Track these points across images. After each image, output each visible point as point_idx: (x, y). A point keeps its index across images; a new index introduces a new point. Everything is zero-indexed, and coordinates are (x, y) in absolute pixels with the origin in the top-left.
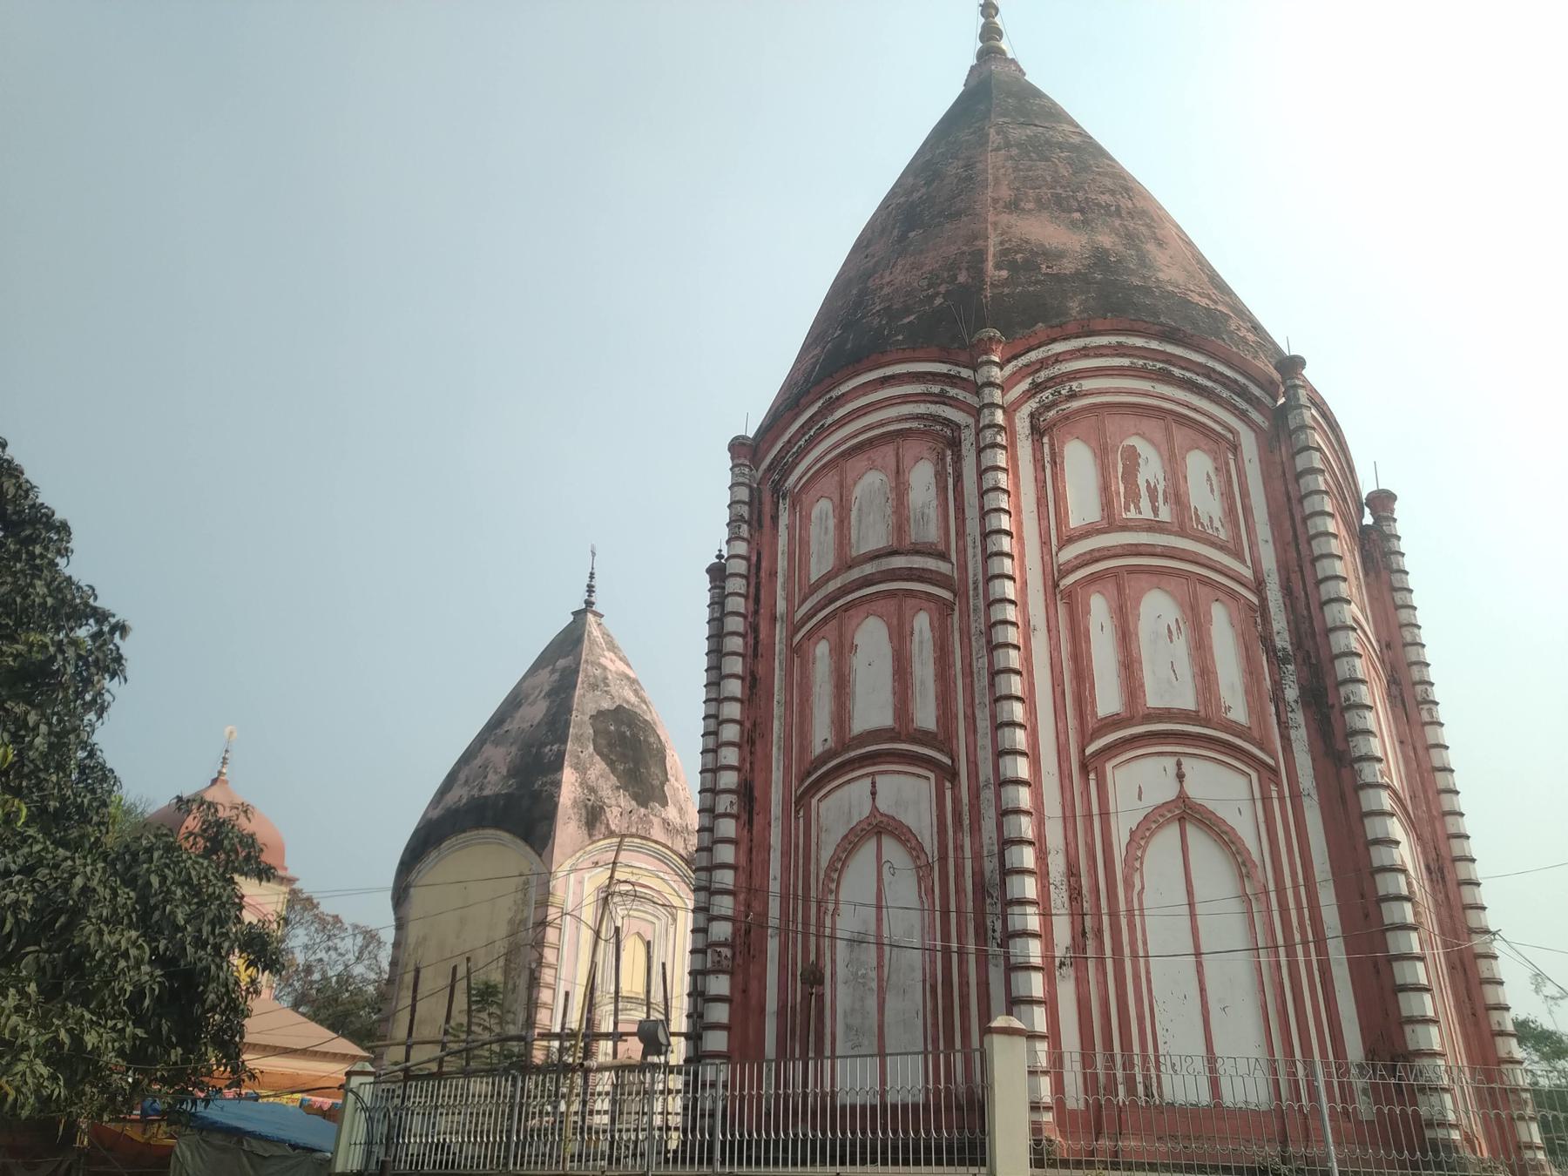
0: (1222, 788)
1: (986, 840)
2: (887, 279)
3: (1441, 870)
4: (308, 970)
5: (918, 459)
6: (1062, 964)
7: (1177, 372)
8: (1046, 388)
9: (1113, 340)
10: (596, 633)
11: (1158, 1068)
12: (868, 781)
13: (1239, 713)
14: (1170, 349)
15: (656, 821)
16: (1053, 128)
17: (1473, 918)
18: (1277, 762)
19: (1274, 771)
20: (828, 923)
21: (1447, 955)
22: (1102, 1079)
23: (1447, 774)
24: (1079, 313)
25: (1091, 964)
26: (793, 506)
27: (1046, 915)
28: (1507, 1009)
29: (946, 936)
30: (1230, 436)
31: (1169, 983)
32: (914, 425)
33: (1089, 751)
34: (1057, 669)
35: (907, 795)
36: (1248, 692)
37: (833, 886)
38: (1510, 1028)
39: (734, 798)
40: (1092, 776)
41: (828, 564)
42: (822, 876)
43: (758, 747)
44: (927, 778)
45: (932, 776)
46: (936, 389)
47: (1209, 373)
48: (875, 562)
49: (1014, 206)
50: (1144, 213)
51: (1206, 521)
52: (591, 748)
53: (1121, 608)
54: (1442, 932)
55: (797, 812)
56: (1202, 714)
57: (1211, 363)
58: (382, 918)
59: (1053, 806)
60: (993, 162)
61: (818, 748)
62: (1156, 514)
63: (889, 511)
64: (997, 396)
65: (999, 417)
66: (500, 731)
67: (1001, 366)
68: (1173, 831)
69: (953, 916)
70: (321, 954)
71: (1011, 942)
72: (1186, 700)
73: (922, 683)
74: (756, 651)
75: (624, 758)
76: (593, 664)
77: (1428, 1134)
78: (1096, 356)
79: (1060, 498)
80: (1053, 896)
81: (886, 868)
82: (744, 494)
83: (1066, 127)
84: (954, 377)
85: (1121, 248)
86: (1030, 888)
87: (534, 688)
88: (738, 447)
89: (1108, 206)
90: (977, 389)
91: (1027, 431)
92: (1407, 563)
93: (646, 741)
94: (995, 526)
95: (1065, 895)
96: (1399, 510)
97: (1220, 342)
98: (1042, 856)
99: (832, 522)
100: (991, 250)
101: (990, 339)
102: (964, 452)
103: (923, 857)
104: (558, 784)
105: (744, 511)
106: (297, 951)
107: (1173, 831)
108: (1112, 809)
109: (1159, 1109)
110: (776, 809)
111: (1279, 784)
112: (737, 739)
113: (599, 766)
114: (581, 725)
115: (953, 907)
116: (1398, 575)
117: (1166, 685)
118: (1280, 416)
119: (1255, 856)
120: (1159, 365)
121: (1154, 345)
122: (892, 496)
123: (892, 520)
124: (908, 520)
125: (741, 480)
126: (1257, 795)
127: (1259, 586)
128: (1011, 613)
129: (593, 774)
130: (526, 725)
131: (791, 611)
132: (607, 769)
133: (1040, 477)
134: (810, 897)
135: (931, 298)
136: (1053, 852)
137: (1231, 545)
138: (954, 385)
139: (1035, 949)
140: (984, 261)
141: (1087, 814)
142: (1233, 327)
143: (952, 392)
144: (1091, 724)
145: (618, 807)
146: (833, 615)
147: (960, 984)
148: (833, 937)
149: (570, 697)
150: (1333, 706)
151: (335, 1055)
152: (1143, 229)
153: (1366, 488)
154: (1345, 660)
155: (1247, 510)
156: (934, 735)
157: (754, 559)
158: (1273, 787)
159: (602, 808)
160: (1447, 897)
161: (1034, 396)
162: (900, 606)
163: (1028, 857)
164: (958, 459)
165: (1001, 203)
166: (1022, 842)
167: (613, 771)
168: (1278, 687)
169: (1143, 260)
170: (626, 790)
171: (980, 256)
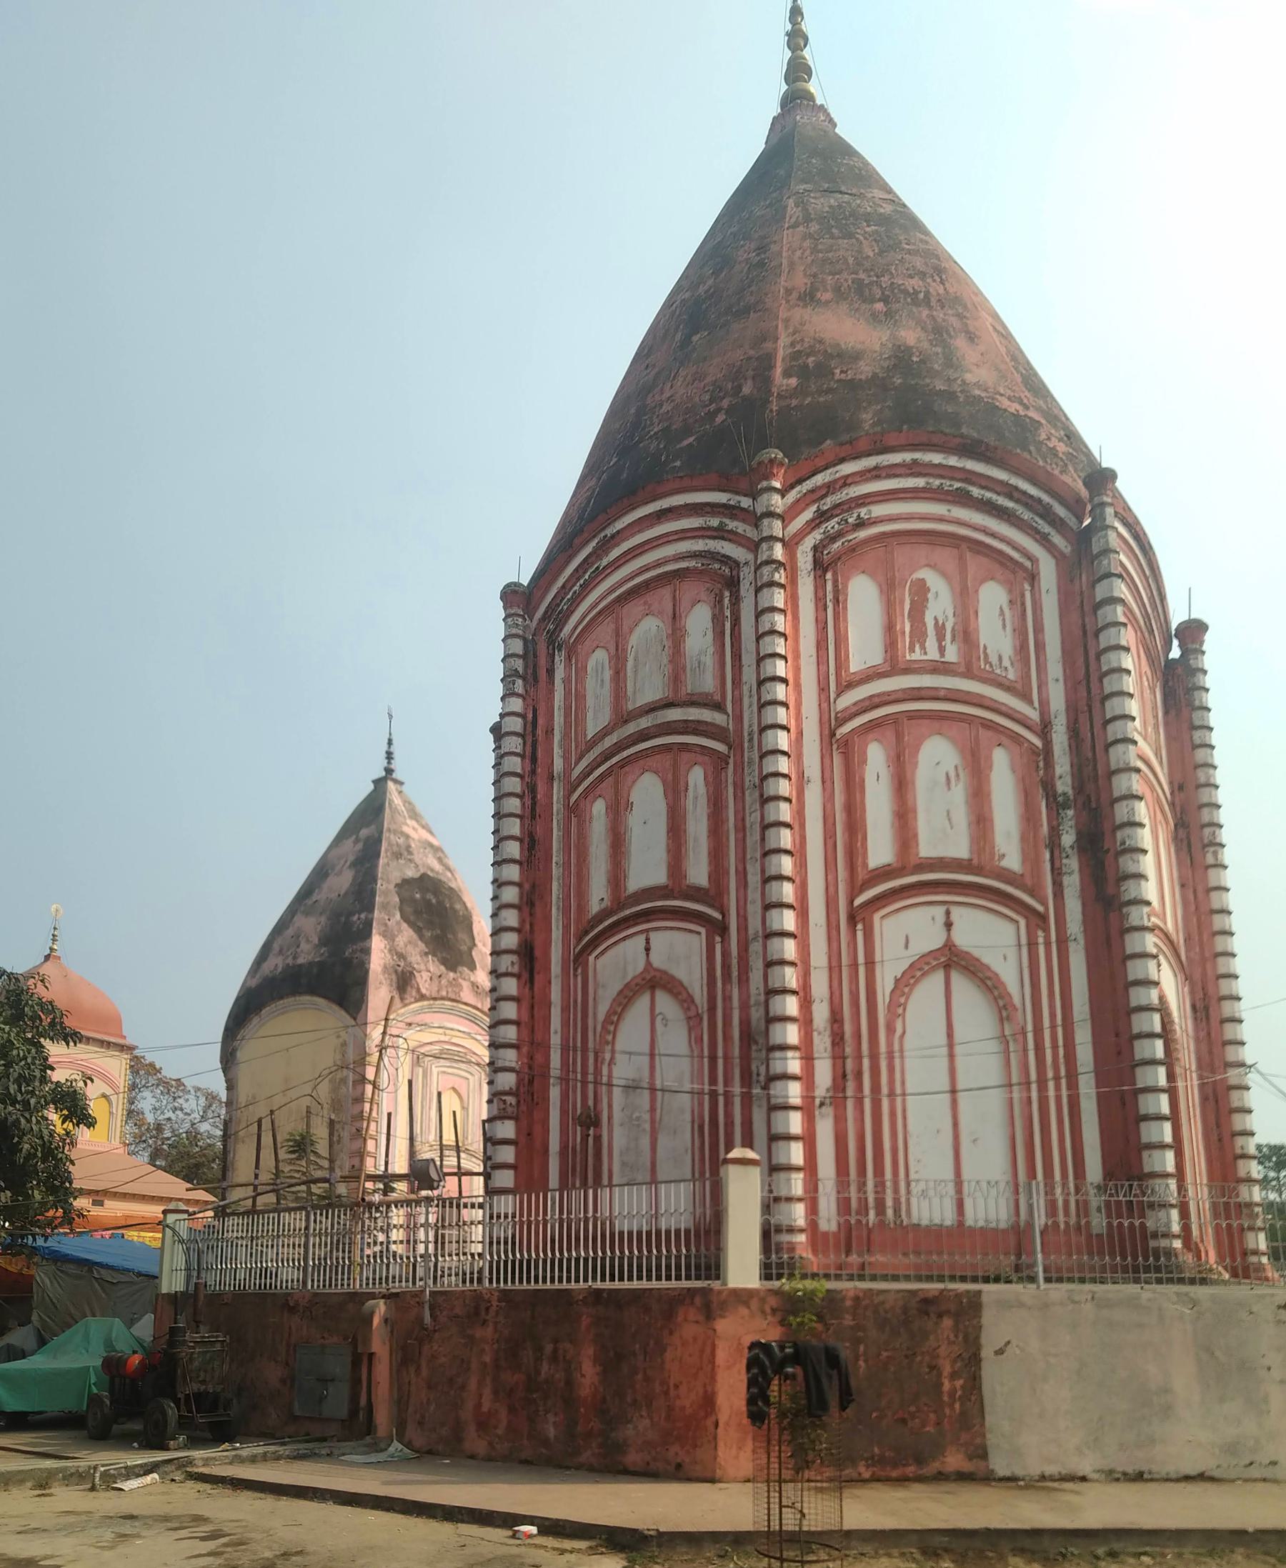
0: (990, 935)
1: (753, 990)
2: (666, 395)
3: (1207, 1009)
4: (159, 1128)
6: (822, 1104)
7: (976, 492)
8: (833, 516)
9: (907, 457)
10: (397, 801)
12: (642, 938)
13: (1013, 861)
14: (971, 465)
15: (465, 984)
16: (861, 196)
17: (1231, 1054)
18: (1047, 909)
19: (1043, 918)
20: (605, 1071)
21: (1202, 1086)
22: (854, 1204)
23: (1225, 916)
25: (850, 1104)
26: (569, 658)
27: (808, 1059)
28: (1253, 1134)
29: (713, 1081)
30: (1028, 564)
31: (924, 1122)
32: (691, 564)
33: (857, 902)
34: (830, 821)
35: (679, 950)
36: (1024, 838)
37: (610, 1038)
38: (1252, 1150)
39: (514, 958)
40: (860, 926)
42: (599, 1028)
43: (538, 910)
44: (699, 933)
45: (703, 930)
46: (715, 522)
47: (1011, 492)
48: (651, 716)
49: (809, 297)
51: (994, 659)
52: (398, 916)
53: (898, 757)
54: (1200, 1067)
55: (575, 970)
56: (975, 862)
57: (1014, 481)
58: (217, 1084)
59: (819, 957)
60: (791, 244)
61: (595, 907)
62: (942, 655)
63: (665, 661)
64: (777, 528)
65: (778, 552)
66: (309, 902)
67: (783, 492)
68: (939, 977)
70: (170, 1114)
71: (772, 1085)
72: (960, 848)
73: (696, 840)
74: (533, 812)
75: (430, 924)
76: (395, 832)
77: (1152, 1244)
78: (889, 476)
79: (841, 640)
81: (659, 1019)
82: (518, 647)
83: (878, 194)
84: (733, 507)
85: (926, 345)
86: (792, 1034)
88: (511, 595)
89: (916, 293)
90: (755, 519)
91: (810, 566)
92: (1211, 700)
94: (769, 673)
97: (1026, 455)
98: (806, 1004)
99: (608, 674)
100: (781, 354)
101: (772, 461)
102: (743, 593)
103: (693, 1008)
104: (367, 951)
105: (519, 664)
107: (939, 977)
108: (878, 958)
109: (905, 1229)
111: (1046, 930)
113: (406, 935)
114: (386, 893)
116: (1199, 713)
117: (943, 835)
118: (1083, 539)
119: (1017, 1000)
120: (957, 485)
121: (953, 461)
122: (668, 643)
123: (668, 670)
125: (514, 631)
126: (1024, 941)
127: (1044, 729)
128: (783, 765)
129: (401, 941)
130: (334, 896)
131: (568, 769)
132: (415, 936)
133: (821, 616)
134: (588, 1049)
137: (1019, 686)
138: (733, 517)
139: (794, 1092)
140: (771, 367)
141: (853, 966)
142: (1043, 436)
143: (732, 525)
145: (427, 971)
147: (726, 1124)
148: (610, 1085)
149: (375, 866)
150: (1108, 850)
151: (125, 1194)
152: (954, 321)
153: (1177, 617)
154: (1125, 803)
155: (1040, 646)
156: (706, 891)
157: (530, 716)
158: (1040, 933)
159: (411, 973)
160: (1209, 1034)
161: (818, 526)
162: (675, 762)
163: (791, 1006)
164: (736, 600)
165: (795, 295)
166: (785, 991)
167: (421, 937)
168: (1055, 833)
169: (950, 361)
170: (434, 955)
171: (766, 362)
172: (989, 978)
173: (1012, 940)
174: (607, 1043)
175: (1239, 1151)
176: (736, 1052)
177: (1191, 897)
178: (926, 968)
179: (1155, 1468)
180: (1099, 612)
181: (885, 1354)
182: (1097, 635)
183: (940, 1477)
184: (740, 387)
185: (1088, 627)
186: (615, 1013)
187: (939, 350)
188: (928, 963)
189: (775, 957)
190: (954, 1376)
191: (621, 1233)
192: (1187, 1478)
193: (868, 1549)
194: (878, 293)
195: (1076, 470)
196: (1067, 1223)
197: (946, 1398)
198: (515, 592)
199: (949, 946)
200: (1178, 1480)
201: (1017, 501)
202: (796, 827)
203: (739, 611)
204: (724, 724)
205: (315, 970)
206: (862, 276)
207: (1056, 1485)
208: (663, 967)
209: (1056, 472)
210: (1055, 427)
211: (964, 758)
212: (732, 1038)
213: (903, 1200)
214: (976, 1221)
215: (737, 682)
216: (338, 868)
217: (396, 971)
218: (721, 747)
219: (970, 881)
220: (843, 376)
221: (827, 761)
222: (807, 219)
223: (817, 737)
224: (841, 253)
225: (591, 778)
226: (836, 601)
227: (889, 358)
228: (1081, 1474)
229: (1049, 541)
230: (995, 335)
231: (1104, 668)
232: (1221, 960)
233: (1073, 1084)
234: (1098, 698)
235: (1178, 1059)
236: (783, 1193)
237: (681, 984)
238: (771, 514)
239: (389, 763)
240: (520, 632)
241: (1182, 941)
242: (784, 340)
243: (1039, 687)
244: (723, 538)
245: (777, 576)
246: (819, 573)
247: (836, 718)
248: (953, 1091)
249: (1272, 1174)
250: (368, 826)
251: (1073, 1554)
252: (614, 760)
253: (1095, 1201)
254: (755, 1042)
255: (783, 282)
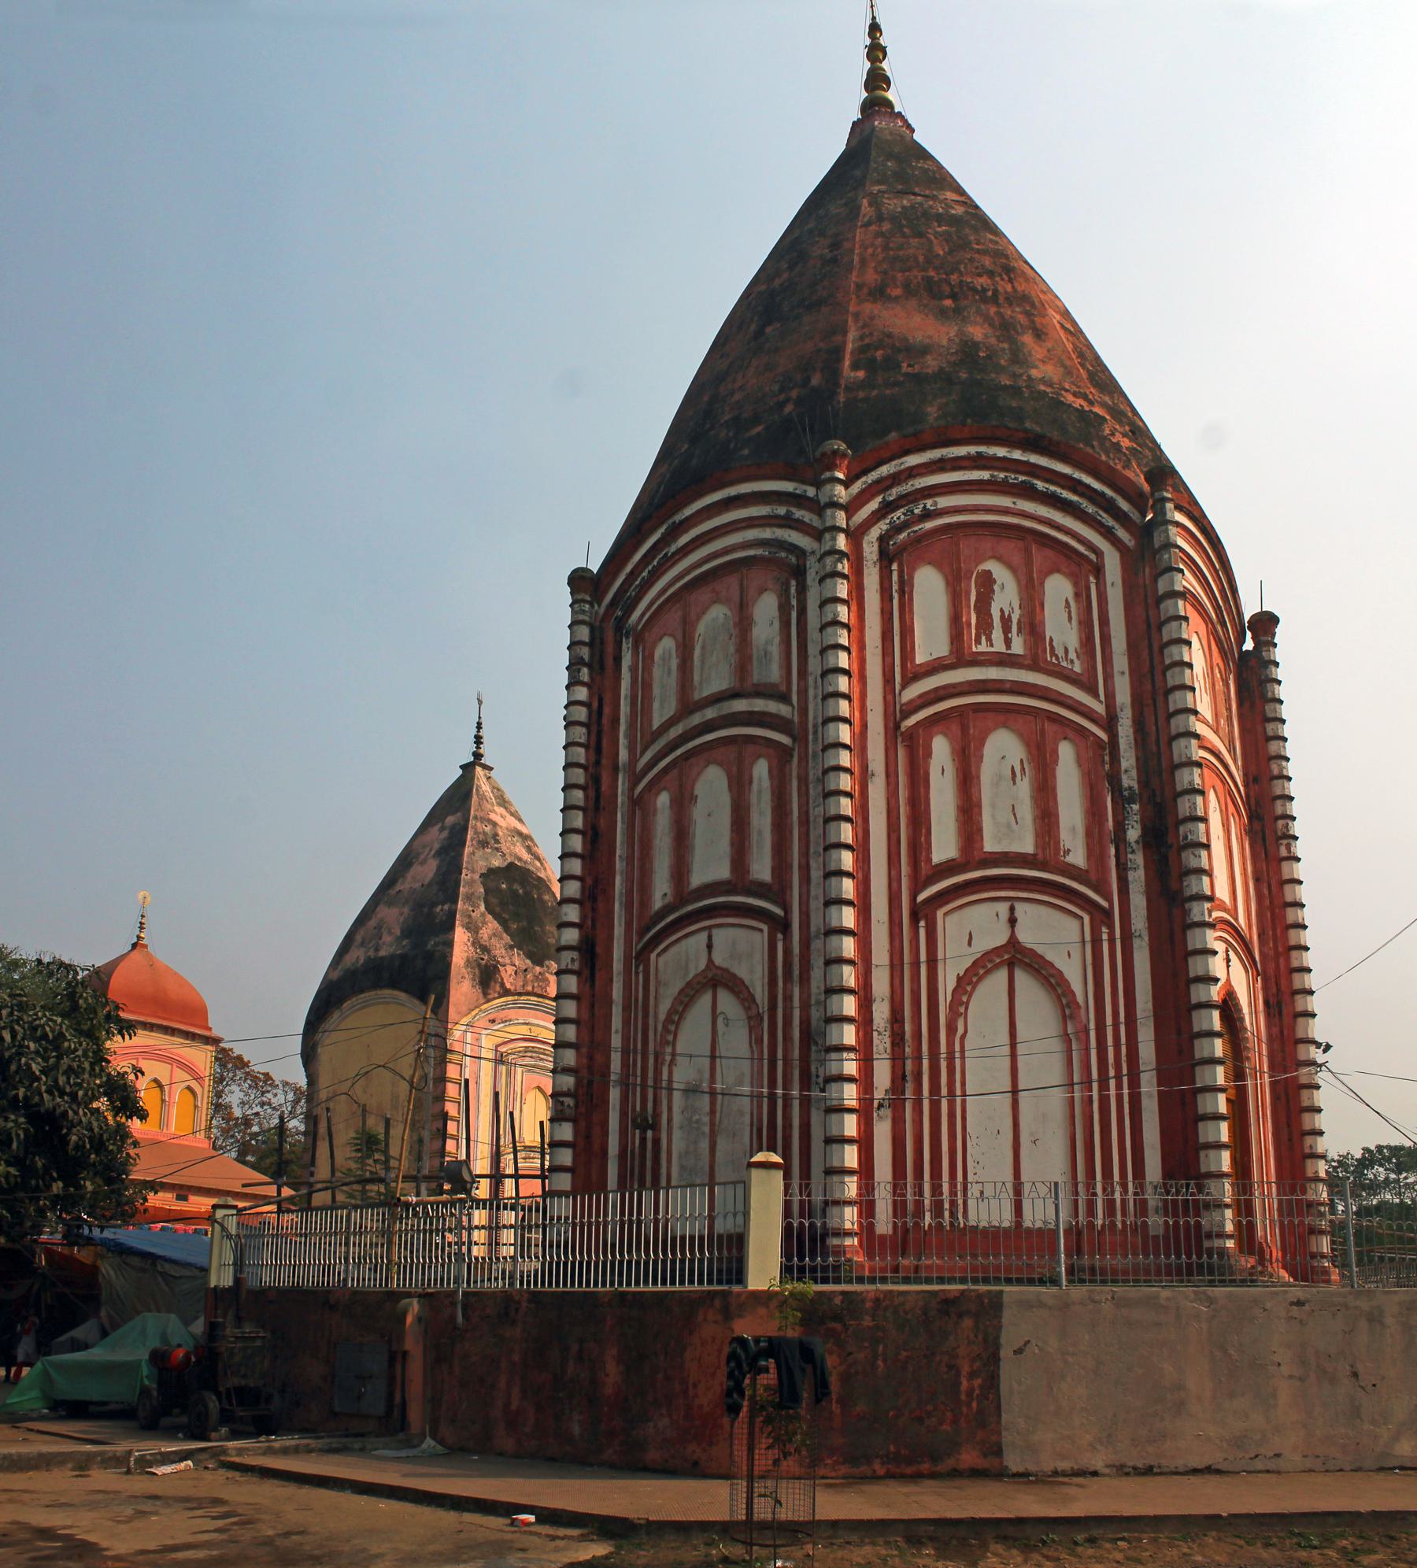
0: (1054, 932)
2: (739, 384)
3: (1279, 1004)
5: (762, 590)
6: (880, 1106)
7: (1040, 485)
9: (972, 450)
10: (485, 787)
11: (965, 1194)
12: (704, 936)
13: (1077, 857)
14: (1034, 459)
16: (934, 198)
19: (1108, 914)
20: (665, 1076)
22: (910, 1207)
24: (936, 419)
25: (908, 1106)
29: (772, 1084)
30: (1093, 557)
32: (759, 552)
33: (921, 897)
35: (742, 948)
36: (1089, 834)
39: (575, 955)
40: (922, 923)
41: (671, 709)
42: (660, 1028)
46: (782, 511)
49: (879, 293)
50: (1025, 299)
51: (1060, 652)
52: (483, 908)
53: (963, 750)
54: (1271, 1067)
55: (637, 967)
56: (1040, 856)
57: (1077, 475)
61: (658, 903)
63: (732, 649)
64: (841, 518)
65: (842, 542)
66: (392, 892)
67: (847, 484)
68: (1002, 975)
69: (780, 1064)
70: (258, 1109)
72: (1026, 845)
73: (760, 833)
77: (1206, 1244)
79: (907, 632)
80: (876, 1041)
81: (720, 1020)
82: (584, 633)
83: (950, 195)
85: (993, 341)
87: (424, 847)
88: (579, 580)
89: (984, 290)
90: (819, 508)
91: (875, 557)
93: (540, 899)
95: (888, 1040)
96: (1281, 634)
97: (1089, 450)
99: (674, 663)
100: (850, 346)
101: (835, 453)
104: (450, 944)
105: (585, 652)
106: (234, 1106)
107: (1002, 975)
108: (940, 956)
110: (617, 965)
111: (1111, 928)
112: (578, 896)
113: (491, 926)
115: (780, 1055)
117: (1008, 829)
118: (1145, 533)
119: (1080, 998)
120: (1022, 478)
121: (1017, 455)
124: (750, 658)
125: (581, 617)
126: (1088, 937)
127: (1110, 722)
128: (845, 758)
130: (417, 885)
131: (633, 759)
132: (500, 929)
134: (651, 1046)
135: (781, 405)
136: (878, 1000)
137: (1084, 679)
138: (800, 506)
140: (839, 359)
141: (915, 962)
142: (1107, 432)
143: (799, 514)
144: (924, 869)
145: (512, 965)
146: (674, 763)
152: (1022, 318)
153: (1250, 609)
154: (1187, 797)
157: (595, 705)
158: (1104, 930)
159: (495, 967)
160: (1282, 1032)
161: (884, 517)
164: (802, 590)
165: (865, 290)
167: (507, 930)
169: (1018, 357)
171: (837, 353)
172: (1052, 976)
173: (1075, 936)
174: (668, 1043)
175: (1307, 1151)
176: (796, 1053)
177: (1266, 892)
178: (989, 966)
179: (1164, 1462)
180: (1162, 606)
181: (904, 1354)
182: (1160, 630)
183: (955, 1474)
184: (808, 379)
185: (1152, 620)
186: (676, 1012)
187: (1006, 346)
188: (991, 961)
189: (833, 955)
190: (972, 1375)
191: (683, 1238)
192: (1195, 1471)
193: (855, 1538)
194: (947, 289)
195: (1139, 465)
196: (1124, 1223)
197: (963, 1397)
198: (583, 578)
199: (1013, 942)
200: (1186, 1473)
201: (1081, 495)
202: (860, 822)
203: (805, 600)
204: (789, 716)
205: (397, 963)
206: (932, 273)
207: (1066, 1480)
208: (724, 965)
209: (1119, 467)
210: (1121, 423)
211: (1030, 752)
212: (791, 1039)
213: (960, 1202)
214: (1034, 1222)
215: (803, 673)
216: (422, 857)
217: (479, 965)
218: (785, 740)
219: (1035, 876)
220: (910, 370)
221: (891, 753)
222: (880, 218)
223: (881, 730)
224: (911, 251)
225: (655, 771)
226: (902, 592)
227: (956, 353)
228: (1092, 1469)
229: (1114, 535)
230: (1062, 333)
231: (1167, 662)
232: (1294, 954)
233: (1135, 1083)
234: (1161, 691)
235: (1248, 1058)
236: (837, 1196)
237: (742, 982)
238: (834, 505)
239: (478, 748)
240: (587, 618)
241: (1255, 937)
242: (852, 335)
243: (1105, 681)
244: (790, 527)
245: (840, 566)
246: (885, 563)
247: (901, 711)
248: (1015, 1091)
249: (1393, 1176)
250: (453, 814)
251: (1053, 1541)
252: (679, 752)
253: (1153, 1200)
254: (814, 1041)
255: (854, 277)
